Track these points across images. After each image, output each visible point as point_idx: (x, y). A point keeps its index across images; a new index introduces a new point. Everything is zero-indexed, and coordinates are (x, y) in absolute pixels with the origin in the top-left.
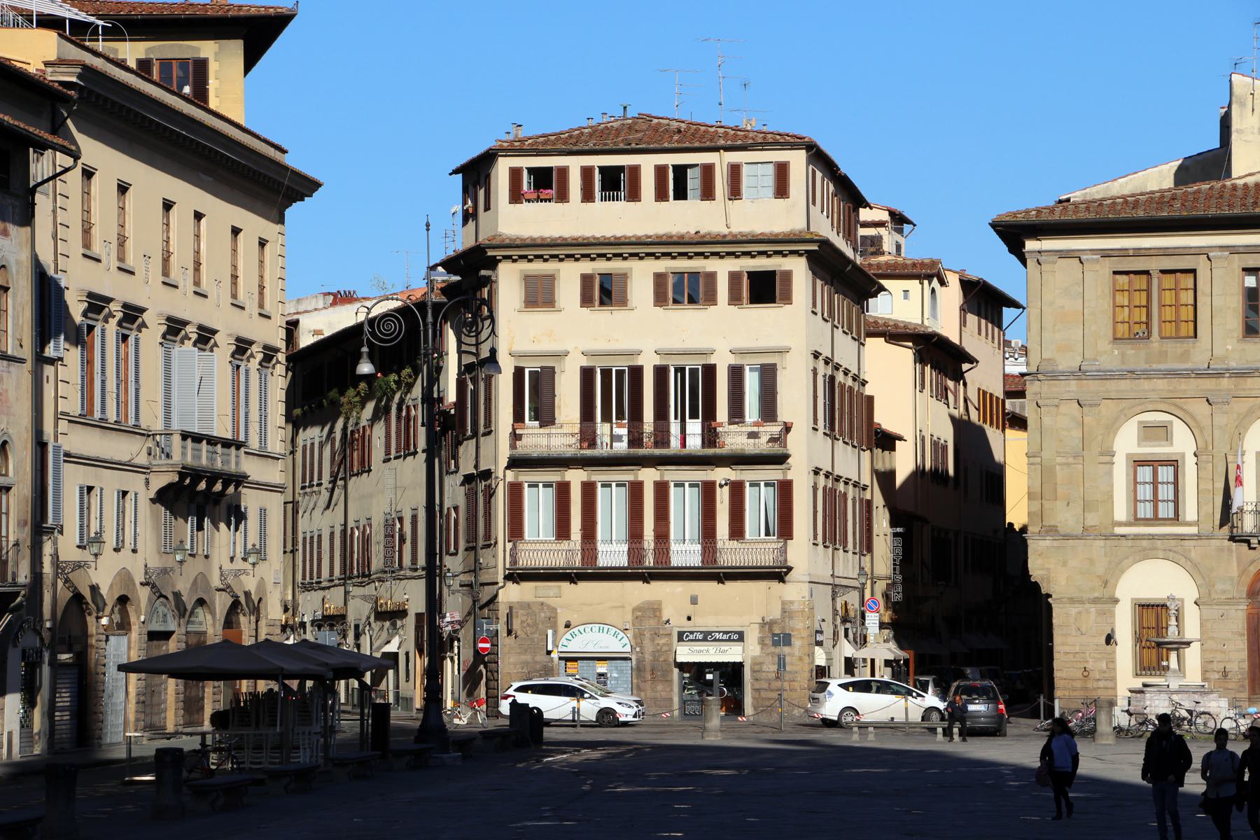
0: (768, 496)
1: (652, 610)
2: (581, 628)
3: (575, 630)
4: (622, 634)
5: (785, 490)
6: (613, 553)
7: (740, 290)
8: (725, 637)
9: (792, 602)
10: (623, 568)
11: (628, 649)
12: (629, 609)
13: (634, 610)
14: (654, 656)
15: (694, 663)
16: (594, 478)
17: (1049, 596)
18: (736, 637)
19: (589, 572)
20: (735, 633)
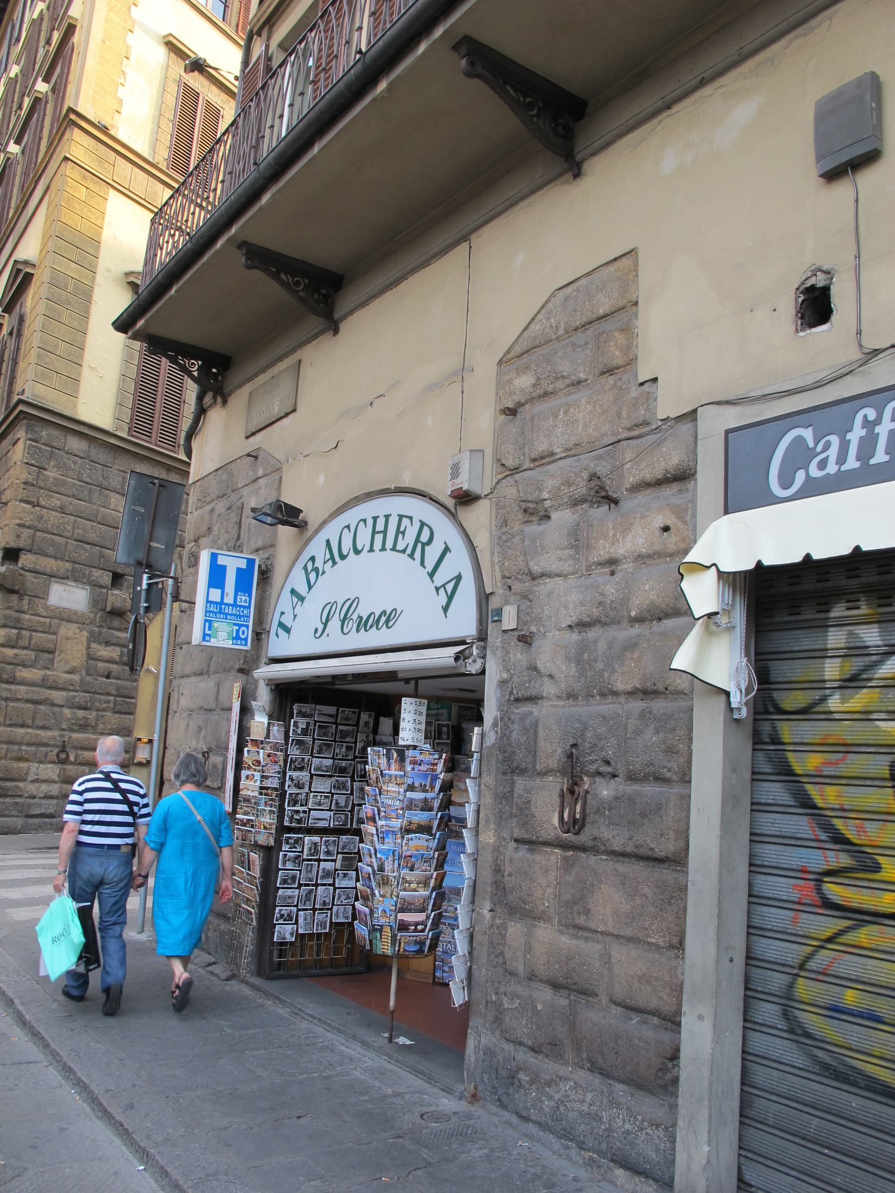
4: (445, 531)
11: (463, 621)
13: (512, 360)
14: (581, 657)
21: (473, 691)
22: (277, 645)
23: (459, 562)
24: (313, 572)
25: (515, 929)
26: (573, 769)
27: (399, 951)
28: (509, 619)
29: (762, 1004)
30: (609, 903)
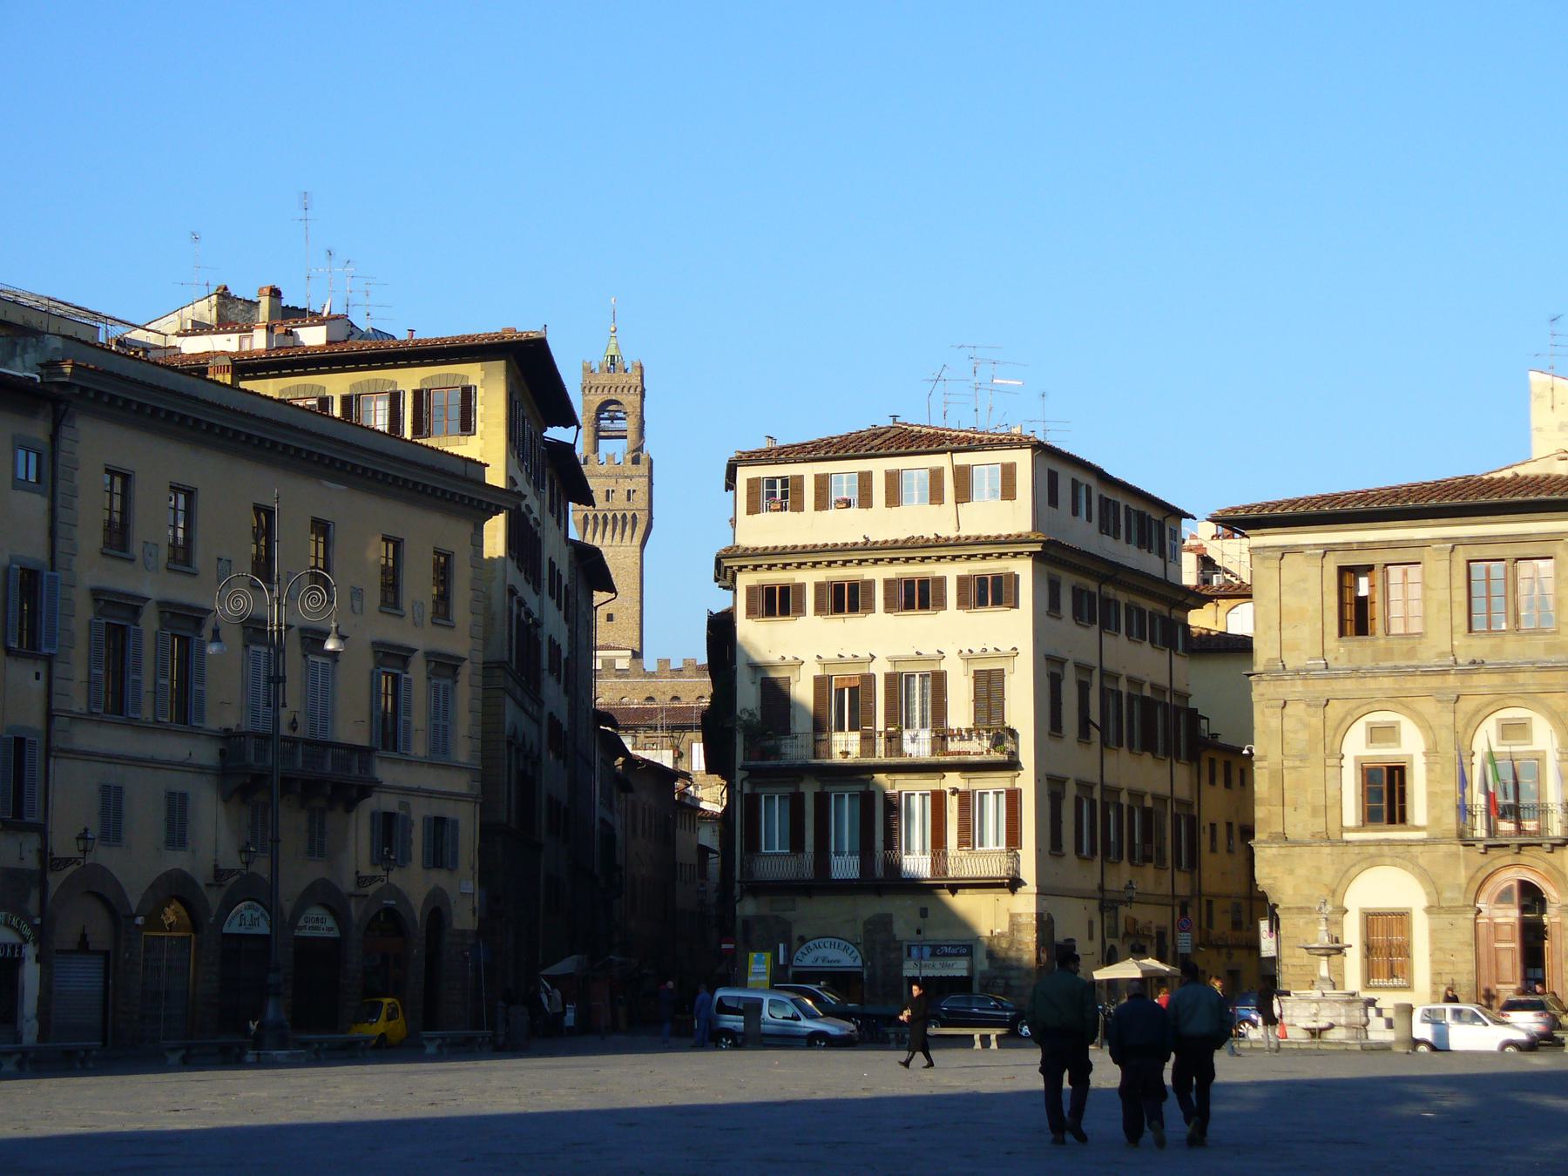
1: (882, 924)
3: (810, 944)
5: (1013, 797)
6: (845, 866)
8: (954, 951)
9: (1020, 915)
11: (859, 962)
13: (865, 923)
18: (964, 951)
19: (822, 884)
23: (856, 953)
24: (809, 949)
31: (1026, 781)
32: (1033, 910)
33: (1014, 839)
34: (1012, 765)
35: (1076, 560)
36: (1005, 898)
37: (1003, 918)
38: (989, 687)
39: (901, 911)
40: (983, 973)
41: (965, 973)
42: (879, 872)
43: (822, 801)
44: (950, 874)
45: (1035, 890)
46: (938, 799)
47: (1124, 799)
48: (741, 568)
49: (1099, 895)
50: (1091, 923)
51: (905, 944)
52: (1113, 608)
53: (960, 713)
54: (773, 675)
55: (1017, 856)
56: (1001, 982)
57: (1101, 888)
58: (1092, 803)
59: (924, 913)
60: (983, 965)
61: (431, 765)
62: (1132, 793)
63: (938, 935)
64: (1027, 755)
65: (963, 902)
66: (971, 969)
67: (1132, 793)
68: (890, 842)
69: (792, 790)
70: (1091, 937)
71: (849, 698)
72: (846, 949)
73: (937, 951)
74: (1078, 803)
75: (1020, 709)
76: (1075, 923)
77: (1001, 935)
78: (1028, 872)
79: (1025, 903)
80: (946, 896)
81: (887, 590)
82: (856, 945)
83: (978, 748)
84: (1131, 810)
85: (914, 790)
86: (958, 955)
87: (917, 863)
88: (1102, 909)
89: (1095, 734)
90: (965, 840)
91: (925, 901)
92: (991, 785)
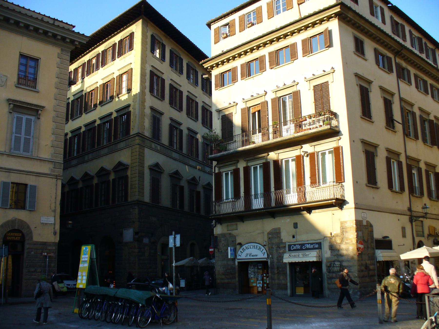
0: (329, 160)
1: (275, 234)
2: (247, 245)
3: (244, 247)
4: (262, 248)
5: (337, 152)
6: (258, 204)
7: (426, 136)
8: (312, 247)
9: (346, 222)
10: (240, 212)
11: (266, 256)
12: (266, 233)
13: (269, 234)
14: (277, 259)
15: (299, 263)
16: (250, 164)
17: (384, 237)
18: (317, 246)
19: (248, 215)
20: (317, 243)
21: (256, 256)
22: (238, 257)
23: (264, 251)
24: (244, 250)
25: (273, 281)
26: (278, 268)
27: (392, 295)
28: (271, 256)
29: (49, 158)
30: (281, 278)
31: (344, 142)
32: (354, 218)
33: (339, 177)
34: (334, 133)
35: (372, 30)
36: (336, 211)
37: (338, 227)
38: (321, 93)
39: (284, 224)
40: (327, 259)
41: (315, 259)
42: (273, 204)
43: (247, 170)
44: (308, 200)
45: (353, 206)
46: (299, 160)
47: (422, 166)
48: (212, 67)
49: (409, 213)
50: (403, 229)
51: (287, 244)
52: (406, 73)
53: (308, 107)
54: (227, 113)
55: (342, 186)
56: (337, 263)
57: (410, 209)
58: (400, 164)
59: (296, 226)
60: (327, 254)
61: (9, 155)
62: (427, 164)
63: (302, 238)
64: (343, 125)
65: (318, 218)
66: (320, 256)
67: (427, 164)
68: (279, 186)
69: (234, 167)
70: (404, 236)
71: (255, 116)
72: (260, 249)
73: (302, 247)
74: (388, 160)
75: (338, 101)
76: (386, 226)
77: (337, 235)
78: (349, 196)
79: (348, 215)
80: (307, 215)
81: (270, 58)
82: (264, 246)
83: (319, 126)
84: (427, 172)
85: (285, 155)
86: (314, 249)
87: (292, 199)
88: (411, 221)
89: (399, 127)
90: (314, 182)
91: (296, 219)
92: (327, 145)
